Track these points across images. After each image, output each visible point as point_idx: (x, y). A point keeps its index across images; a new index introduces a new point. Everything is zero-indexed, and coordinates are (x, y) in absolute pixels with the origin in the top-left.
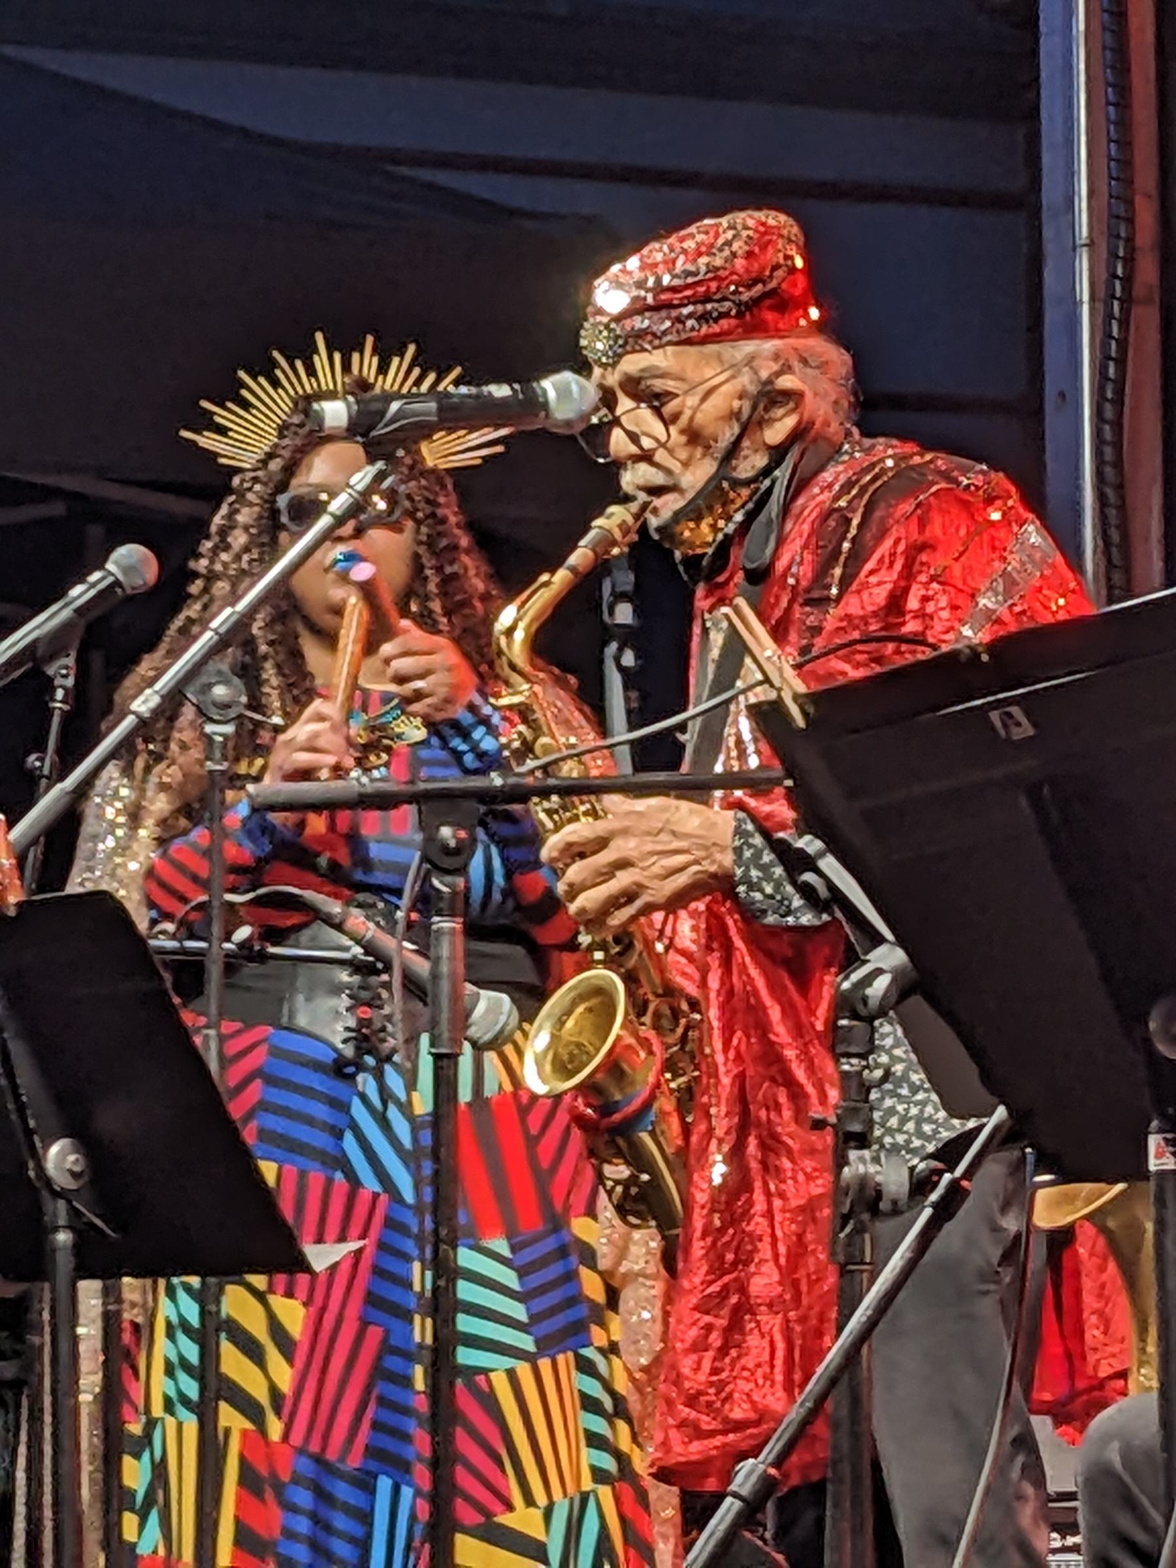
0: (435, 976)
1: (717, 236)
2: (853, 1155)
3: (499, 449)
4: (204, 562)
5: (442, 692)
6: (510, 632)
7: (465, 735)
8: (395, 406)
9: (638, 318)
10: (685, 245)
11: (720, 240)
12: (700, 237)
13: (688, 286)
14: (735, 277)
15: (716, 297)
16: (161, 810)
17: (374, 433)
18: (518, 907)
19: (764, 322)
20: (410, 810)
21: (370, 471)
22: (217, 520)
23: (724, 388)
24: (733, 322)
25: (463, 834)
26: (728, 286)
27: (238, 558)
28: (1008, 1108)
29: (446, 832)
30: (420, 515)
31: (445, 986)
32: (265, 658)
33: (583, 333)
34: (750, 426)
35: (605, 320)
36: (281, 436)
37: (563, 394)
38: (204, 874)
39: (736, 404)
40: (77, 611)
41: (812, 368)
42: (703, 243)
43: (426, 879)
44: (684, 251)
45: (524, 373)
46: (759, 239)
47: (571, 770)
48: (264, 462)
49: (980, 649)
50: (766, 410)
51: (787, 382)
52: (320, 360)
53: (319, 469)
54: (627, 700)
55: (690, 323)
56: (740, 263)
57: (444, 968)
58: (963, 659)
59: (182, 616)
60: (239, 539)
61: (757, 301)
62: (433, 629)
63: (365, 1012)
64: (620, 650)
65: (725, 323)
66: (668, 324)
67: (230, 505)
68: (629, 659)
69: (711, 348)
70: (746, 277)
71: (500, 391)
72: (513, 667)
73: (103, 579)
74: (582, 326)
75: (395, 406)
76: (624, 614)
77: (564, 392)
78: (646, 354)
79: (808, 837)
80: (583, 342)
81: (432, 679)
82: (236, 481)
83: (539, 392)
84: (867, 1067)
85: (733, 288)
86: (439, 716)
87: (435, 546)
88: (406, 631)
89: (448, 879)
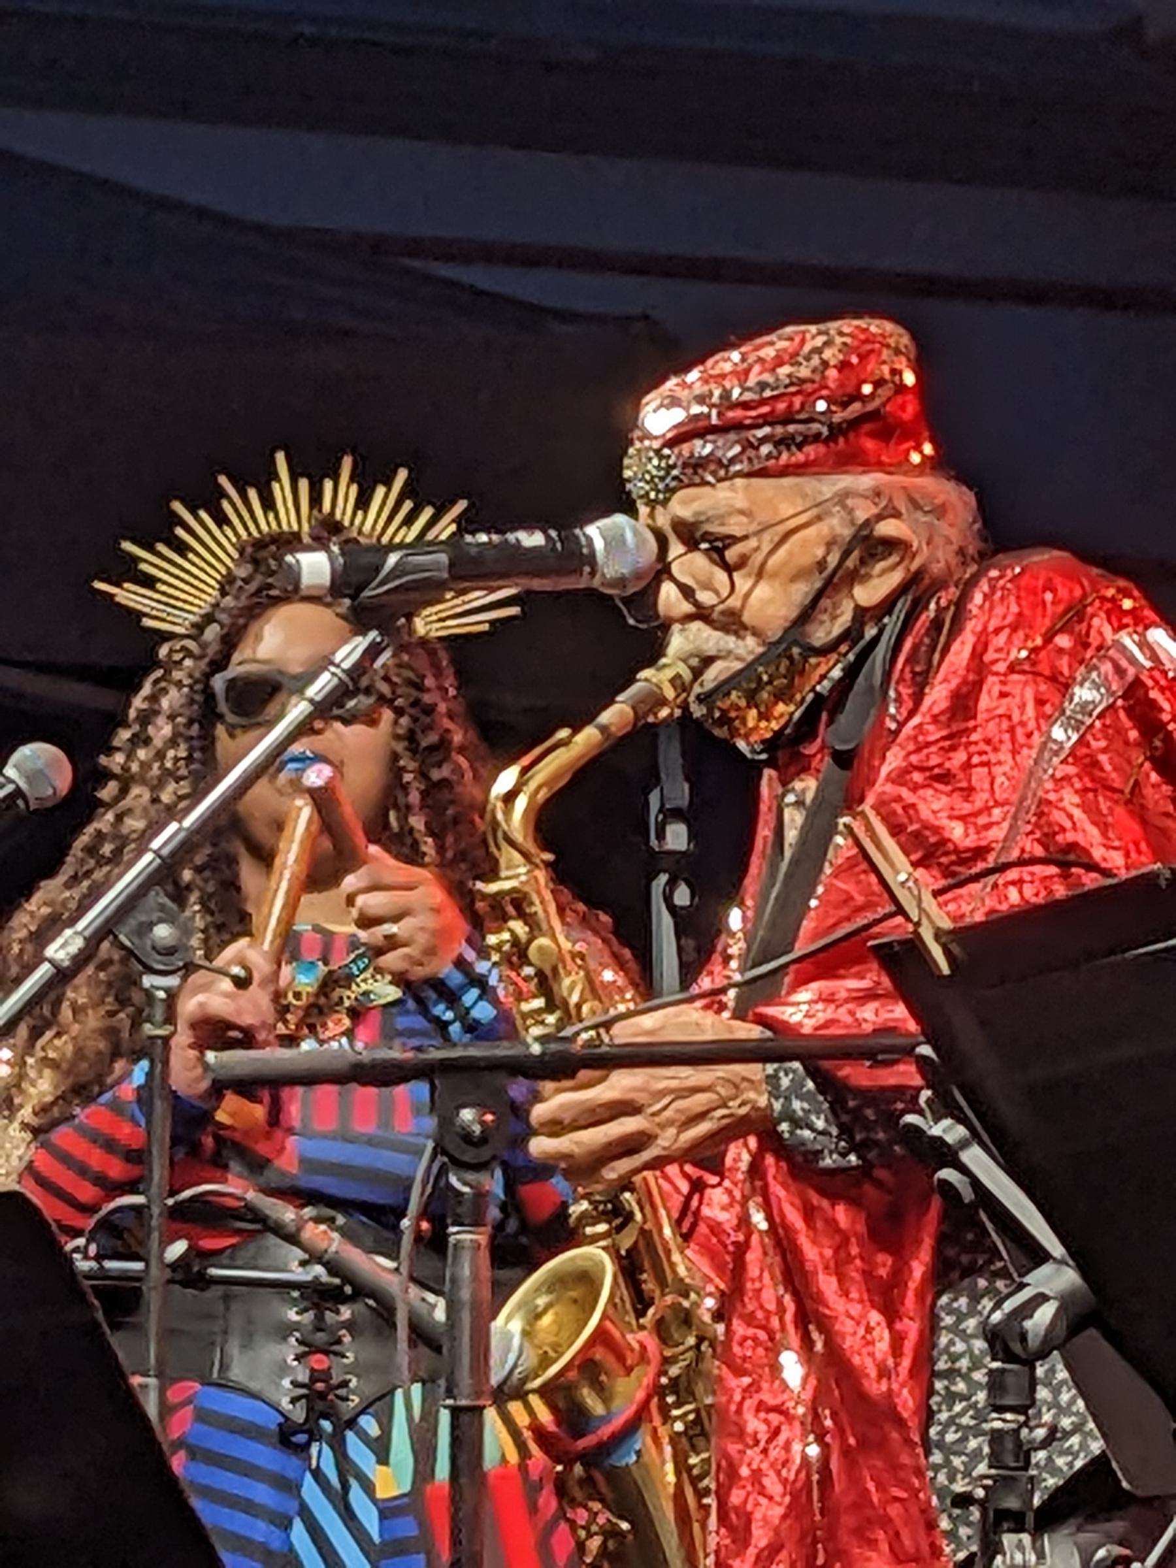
2: (1008, 1540)
3: (514, 611)
4: (119, 758)
5: (422, 939)
7: (452, 998)
8: (393, 559)
9: (698, 443)
10: (762, 353)
11: (806, 350)
13: (763, 402)
14: (825, 392)
15: (803, 416)
16: (42, 1094)
17: (367, 593)
18: (524, 1227)
19: (864, 452)
20: (421, 1089)
21: (360, 644)
22: (138, 702)
24: (822, 449)
27: (160, 755)
30: (399, 702)
32: (189, 888)
33: (626, 462)
34: (834, 582)
35: (656, 444)
36: (224, 593)
37: (613, 542)
39: (820, 552)
41: (921, 507)
42: (785, 350)
43: (443, 1171)
44: (760, 360)
45: (565, 516)
48: (199, 628)
51: (887, 528)
53: (274, 642)
54: (680, 950)
59: (90, 830)
60: (162, 730)
61: (854, 424)
62: (413, 857)
63: (319, 1361)
64: (672, 884)
65: (811, 451)
66: (737, 449)
67: (156, 682)
68: (682, 896)
70: (840, 392)
71: (532, 539)
74: (625, 452)
75: (393, 559)
76: (677, 837)
77: (615, 542)
78: (707, 489)
79: (947, 1122)
80: (627, 474)
81: (407, 924)
82: (163, 651)
83: (583, 540)
84: (1025, 1424)
85: (821, 406)
86: (419, 972)
87: (420, 744)
88: (375, 859)
89: (470, 1176)
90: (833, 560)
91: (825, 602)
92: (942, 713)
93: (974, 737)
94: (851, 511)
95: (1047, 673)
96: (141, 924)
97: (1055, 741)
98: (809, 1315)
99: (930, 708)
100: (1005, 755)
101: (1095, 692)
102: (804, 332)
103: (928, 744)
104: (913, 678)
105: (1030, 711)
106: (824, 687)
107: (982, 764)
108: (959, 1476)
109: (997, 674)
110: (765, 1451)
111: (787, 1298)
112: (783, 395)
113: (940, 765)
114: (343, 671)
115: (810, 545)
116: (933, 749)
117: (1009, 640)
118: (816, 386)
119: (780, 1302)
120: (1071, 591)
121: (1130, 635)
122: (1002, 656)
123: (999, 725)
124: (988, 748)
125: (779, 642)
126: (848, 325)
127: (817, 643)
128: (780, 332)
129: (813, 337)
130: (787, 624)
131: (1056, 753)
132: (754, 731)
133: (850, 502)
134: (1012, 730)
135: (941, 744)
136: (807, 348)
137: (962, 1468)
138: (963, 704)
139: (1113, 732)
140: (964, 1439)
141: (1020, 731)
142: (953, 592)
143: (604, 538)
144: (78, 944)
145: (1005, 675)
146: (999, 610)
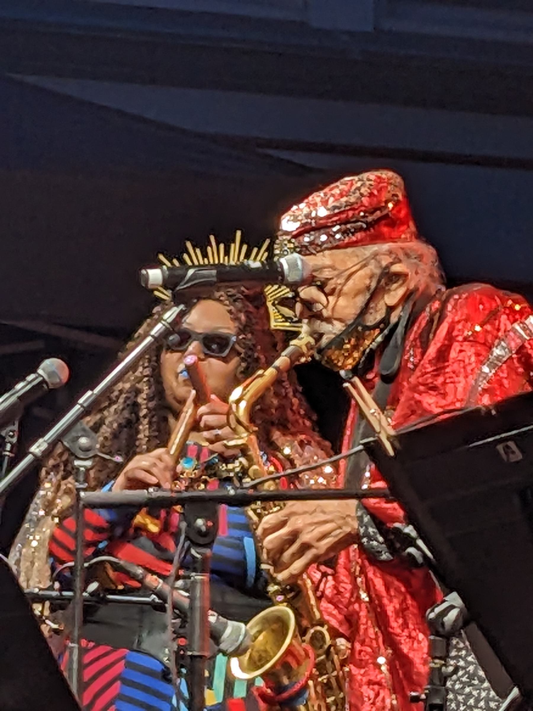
0: (192, 607)
1: (352, 185)
6: (238, 402)
11: (356, 187)
12: (341, 187)
14: (363, 208)
23: (359, 273)
25: (210, 524)
26: (359, 213)
28: (520, 690)
29: (200, 522)
31: (198, 615)
34: (375, 294)
38: (73, 548)
39: (367, 282)
40: (19, 398)
41: (415, 261)
44: (333, 195)
46: (377, 186)
47: (269, 486)
49: (491, 408)
50: (387, 284)
51: (397, 268)
52: (234, 248)
55: (338, 236)
56: (365, 200)
57: (198, 604)
58: (483, 413)
61: (377, 221)
65: (359, 235)
69: (349, 250)
72: (239, 422)
73: (36, 378)
85: (362, 214)
90: (373, 285)
91: (372, 305)
92: (433, 359)
93: (447, 370)
94: (379, 262)
95: (482, 341)
96: (74, 438)
97: (485, 373)
98: (390, 641)
99: (428, 356)
100: (461, 379)
101: (503, 351)
102: (352, 180)
103: (426, 373)
104: (421, 345)
105: (473, 359)
106: (374, 345)
107: (451, 382)
108: (461, 705)
109: (458, 341)
110: (374, 703)
111: (380, 634)
112: (344, 211)
113: (432, 383)
114: (168, 323)
115: (362, 279)
116: (429, 375)
117: (464, 326)
118: (359, 205)
119: (376, 634)
120: (491, 305)
121: (519, 324)
122: (461, 333)
123: (459, 364)
124: (454, 375)
125: (352, 325)
126: (372, 175)
127: (369, 324)
128: (342, 180)
129: (356, 183)
130: (356, 316)
131: (485, 378)
132: (345, 365)
133: (378, 257)
134: (464, 368)
135: (432, 373)
136: (353, 188)
137: (462, 701)
138: (443, 355)
139: (512, 369)
140: (463, 688)
141: (469, 368)
142: (437, 305)
143: (288, 265)
144: (44, 446)
145: (462, 342)
146: (459, 313)
